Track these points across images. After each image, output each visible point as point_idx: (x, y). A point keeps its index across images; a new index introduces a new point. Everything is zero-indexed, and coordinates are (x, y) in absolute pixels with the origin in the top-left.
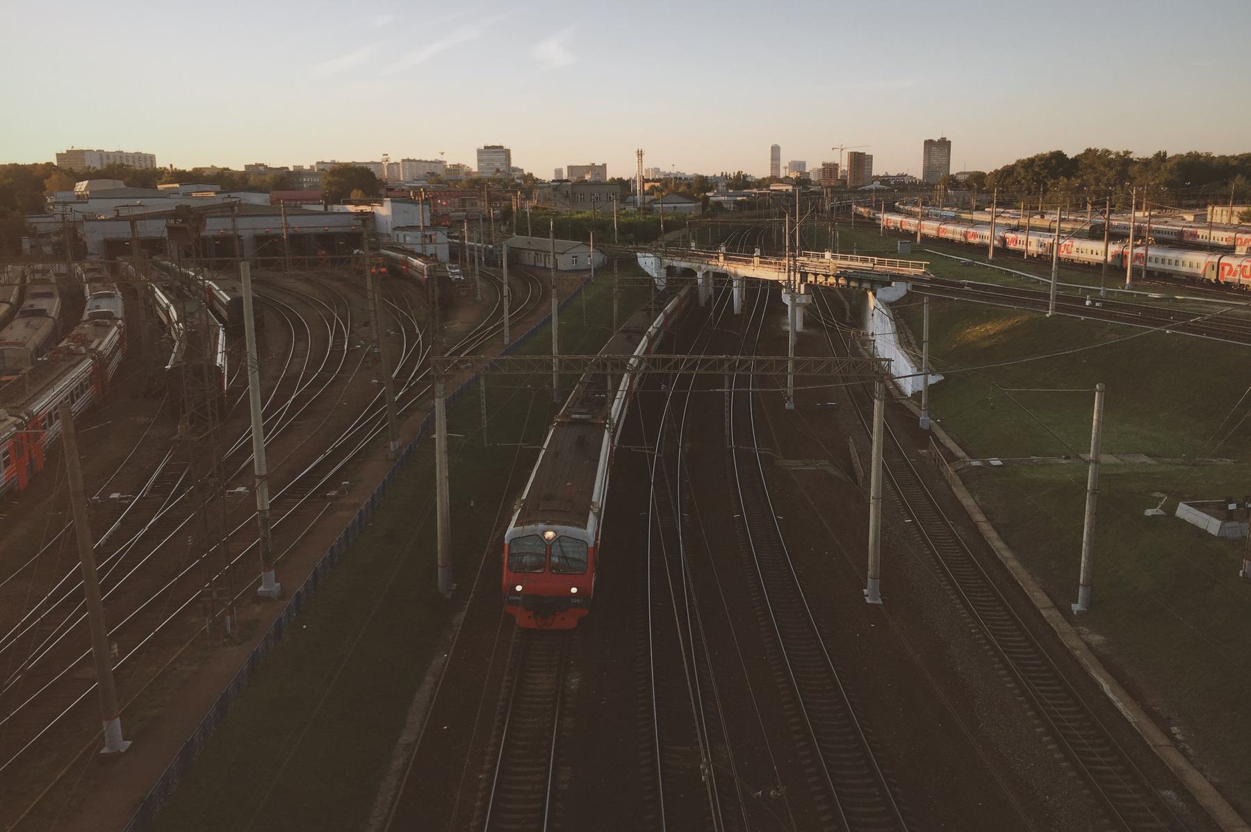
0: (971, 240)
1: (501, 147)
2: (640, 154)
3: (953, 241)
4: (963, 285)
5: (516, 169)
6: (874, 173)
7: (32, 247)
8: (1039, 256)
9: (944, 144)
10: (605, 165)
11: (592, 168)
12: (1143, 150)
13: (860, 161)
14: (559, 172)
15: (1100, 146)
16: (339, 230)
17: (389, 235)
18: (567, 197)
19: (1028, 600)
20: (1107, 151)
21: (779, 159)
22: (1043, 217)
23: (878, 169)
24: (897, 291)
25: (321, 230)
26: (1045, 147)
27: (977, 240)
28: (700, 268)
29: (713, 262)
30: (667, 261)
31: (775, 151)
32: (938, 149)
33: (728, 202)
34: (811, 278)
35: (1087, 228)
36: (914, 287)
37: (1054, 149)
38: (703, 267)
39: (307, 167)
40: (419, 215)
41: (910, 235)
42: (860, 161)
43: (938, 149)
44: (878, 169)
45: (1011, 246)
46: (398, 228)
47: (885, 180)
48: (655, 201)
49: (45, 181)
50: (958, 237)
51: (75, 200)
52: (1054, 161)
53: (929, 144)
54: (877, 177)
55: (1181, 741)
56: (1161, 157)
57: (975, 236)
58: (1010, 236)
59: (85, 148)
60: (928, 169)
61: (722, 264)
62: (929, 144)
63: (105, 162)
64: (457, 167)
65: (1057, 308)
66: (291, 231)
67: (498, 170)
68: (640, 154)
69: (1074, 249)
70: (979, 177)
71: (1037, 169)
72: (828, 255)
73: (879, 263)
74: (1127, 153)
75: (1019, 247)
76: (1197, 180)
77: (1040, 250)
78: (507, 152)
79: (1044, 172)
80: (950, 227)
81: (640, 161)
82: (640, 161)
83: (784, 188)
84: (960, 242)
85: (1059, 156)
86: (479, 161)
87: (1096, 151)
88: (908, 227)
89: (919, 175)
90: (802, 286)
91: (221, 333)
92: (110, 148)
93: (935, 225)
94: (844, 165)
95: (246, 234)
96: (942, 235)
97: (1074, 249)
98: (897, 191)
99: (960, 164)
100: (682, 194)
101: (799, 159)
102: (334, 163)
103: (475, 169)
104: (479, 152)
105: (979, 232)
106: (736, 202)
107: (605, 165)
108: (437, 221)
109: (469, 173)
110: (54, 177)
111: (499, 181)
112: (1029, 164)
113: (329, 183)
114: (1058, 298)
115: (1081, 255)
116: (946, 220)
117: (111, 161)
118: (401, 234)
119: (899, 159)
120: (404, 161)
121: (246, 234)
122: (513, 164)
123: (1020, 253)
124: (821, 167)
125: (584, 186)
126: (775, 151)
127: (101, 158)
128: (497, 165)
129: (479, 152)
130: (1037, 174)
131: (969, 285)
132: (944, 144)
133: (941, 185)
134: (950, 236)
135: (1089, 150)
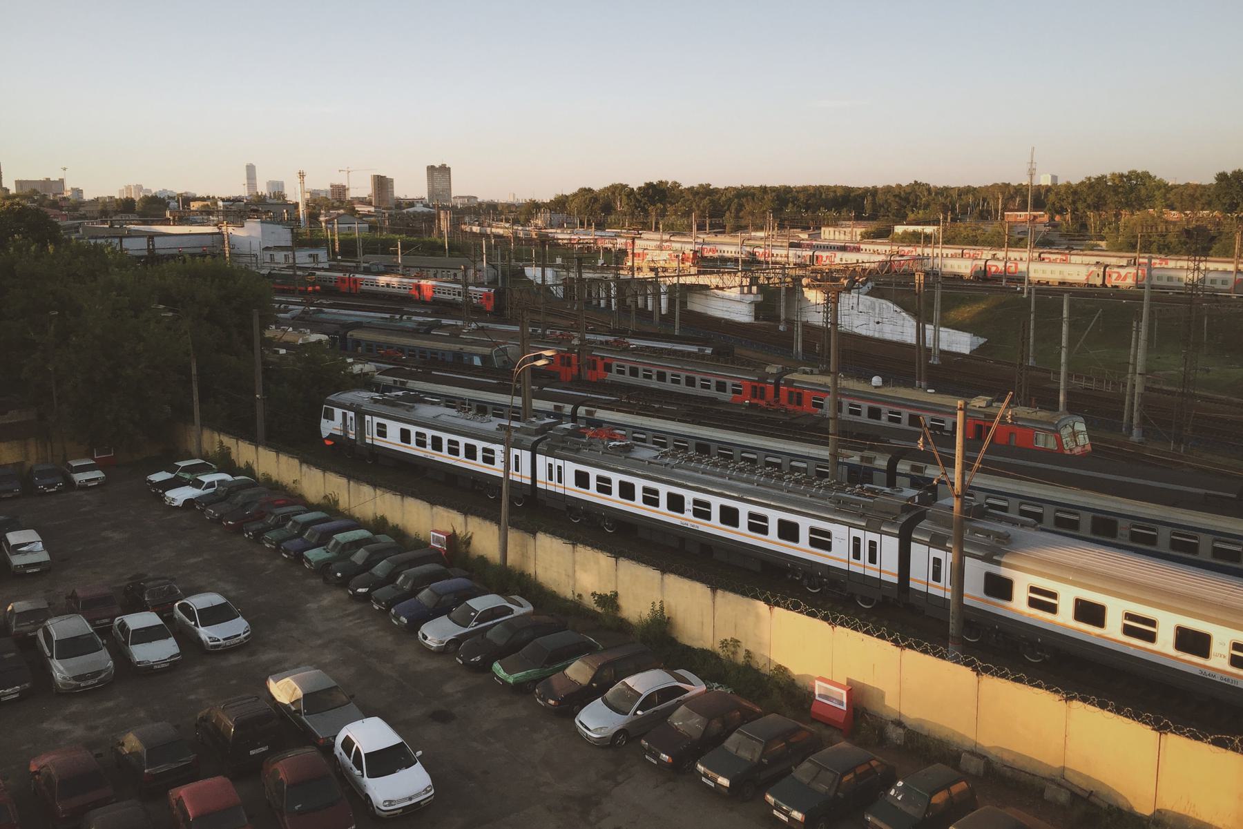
2: (302, 175)
21: (254, 178)
27: (716, 255)
31: (251, 170)
32: (439, 173)
46: (267, 249)
60: (432, 193)
62: (431, 169)
68: (302, 175)
81: (302, 182)
82: (302, 182)
126: (251, 170)
132: (445, 170)
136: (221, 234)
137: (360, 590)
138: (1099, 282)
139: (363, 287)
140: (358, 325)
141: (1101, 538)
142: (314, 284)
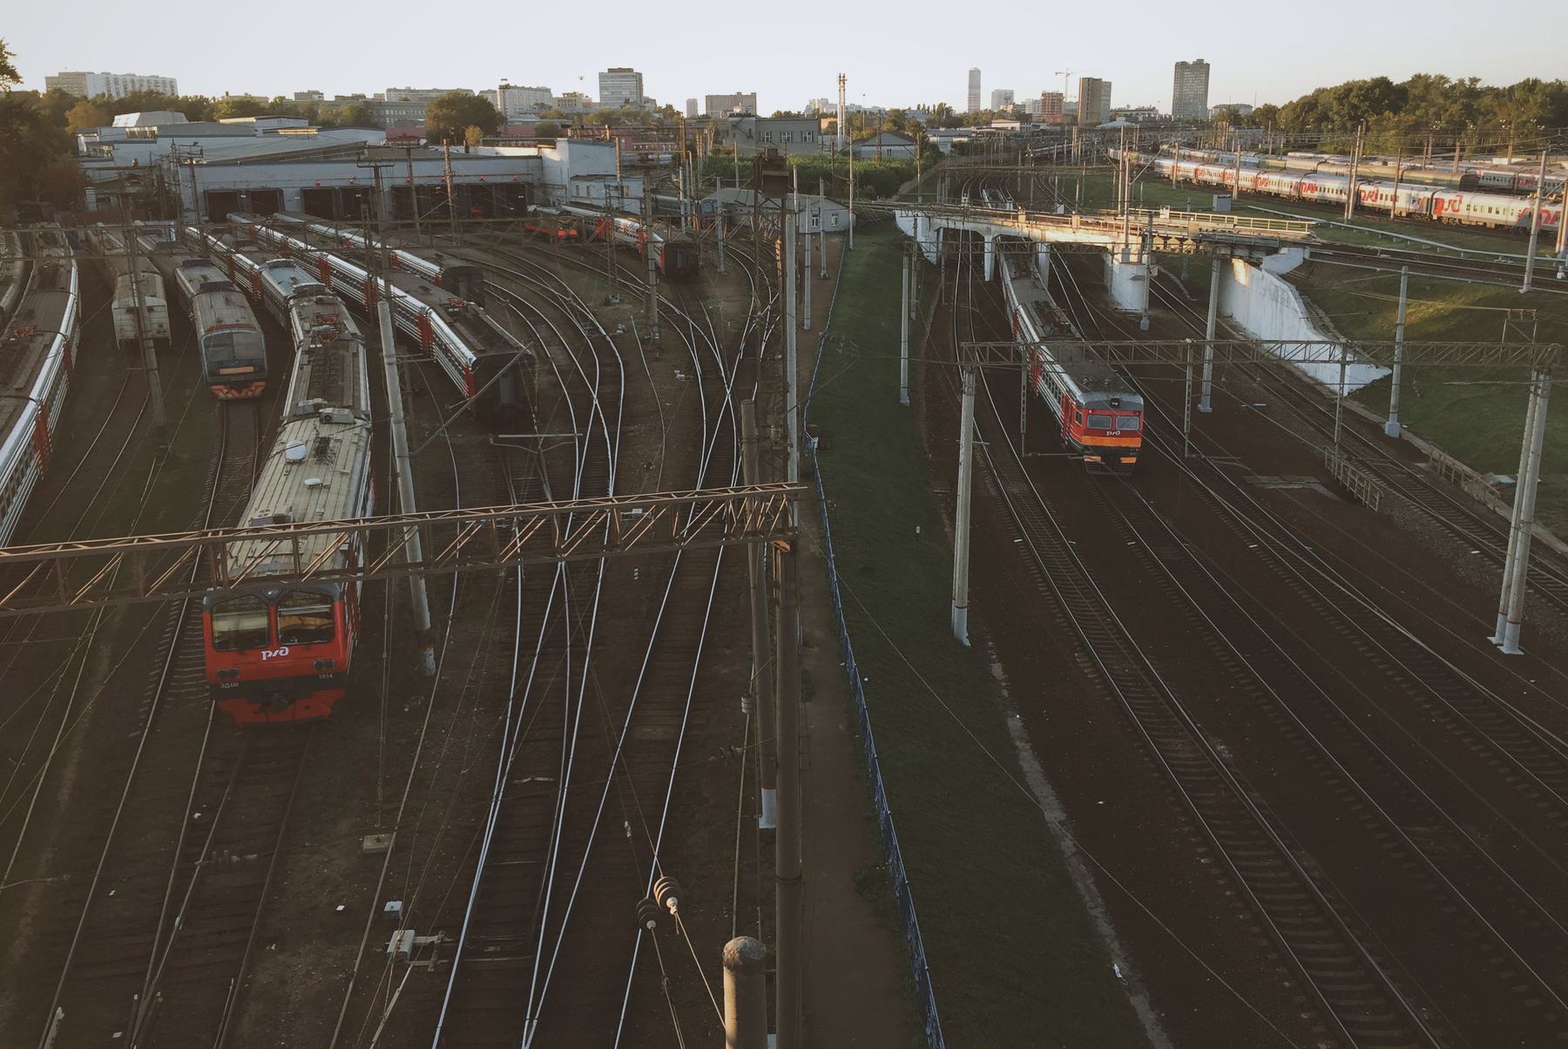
0: (1307, 194)
1: (630, 70)
2: (842, 80)
3: (1277, 195)
4: (1376, 252)
5: (648, 100)
6: (1114, 105)
7: (98, 200)
8: (1409, 215)
9: (1201, 68)
10: (754, 95)
11: (738, 98)
12: (1500, 74)
13: (1094, 89)
14: (692, 104)
15: (1433, 72)
16: (499, 180)
17: (564, 187)
19: (404, 402)
20: (1442, 77)
21: (979, 87)
22: (1385, 163)
23: (1117, 101)
24: (1291, 259)
25: (475, 180)
26: (1366, 73)
27: (1316, 195)
28: (989, 230)
29: (1008, 223)
30: (941, 222)
31: (975, 76)
32: (1192, 74)
33: (945, 143)
34: (1158, 242)
35: (1458, 179)
36: (1312, 254)
37: (1377, 75)
38: (993, 228)
40: (606, 160)
41: (1221, 188)
42: (1094, 89)
43: (1192, 74)
44: (1117, 101)
45: (1368, 202)
46: (577, 177)
47: (1130, 115)
48: (863, 141)
49: (67, 114)
50: (1285, 190)
51: (124, 137)
52: (1377, 91)
53: (1181, 67)
54: (1118, 112)
56: (1531, 86)
57: (1313, 188)
58: (1366, 188)
60: (1179, 102)
61: (1021, 226)
62: (1181, 67)
63: (130, 88)
64: (572, 98)
65: (1534, 282)
66: (457, 181)
67: (627, 101)
68: (842, 80)
69: (1463, 207)
70: (1269, 112)
71: (1355, 101)
72: (1165, 213)
73: (1240, 223)
74: (1474, 80)
75: (1380, 203)
77: (1412, 208)
78: (638, 78)
79: (1364, 106)
80: (1274, 178)
81: (842, 89)
82: (842, 89)
83: (1009, 125)
84: (1290, 196)
85: (1383, 83)
86: (602, 88)
87: (1427, 77)
88: (1207, 178)
89: (1165, 108)
91: (74, 270)
93: (1252, 174)
94: (1073, 95)
96: (1262, 188)
97: (1463, 207)
98: (1149, 131)
99: (1221, 93)
103: (596, 99)
104: (602, 76)
105: (1319, 183)
106: (954, 145)
107: (754, 95)
108: (639, 166)
109: (588, 105)
110: (78, 109)
111: (634, 116)
112: (1346, 93)
113: (436, 117)
114: (1535, 272)
115: (1472, 213)
116: (1204, 161)
117: (137, 86)
118: (583, 185)
119: (1144, 89)
122: (645, 94)
123: (1383, 213)
124: (1039, 97)
125: (734, 118)
126: (975, 76)
127: (108, 83)
128: (626, 94)
129: (602, 76)
130: (1355, 107)
131: (1383, 252)
132: (1201, 68)
133: (1192, 123)
134: (1273, 188)
135: (1418, 77)
136: (539, 158)
137: (249, 857)
138: (1294, 193)
139: (617, 235)
140: (800, 325)
141: (402, 466)
142: (567, 226)
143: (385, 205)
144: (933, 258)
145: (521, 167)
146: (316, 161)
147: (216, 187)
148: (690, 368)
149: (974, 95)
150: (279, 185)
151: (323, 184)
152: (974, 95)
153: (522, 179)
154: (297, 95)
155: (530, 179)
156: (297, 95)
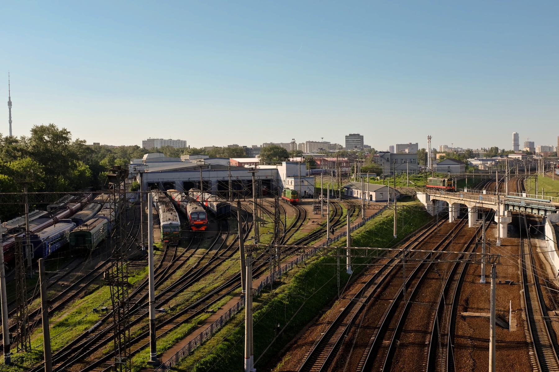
1: (358, 135)
2: (430, 138)
5: (367, 146)
11: (410, 146)
14: (392, 148)
18: (388, 161)
31: (516, 137)
39: (259, 146)
55: (124, 334)
59: (156, 138)
68: (430, 138)
76: (524, 168)
78: (362, 138)
90: (506, 213)
92: (166, 138)
95: (214, 180)
100: (454, 160)
101: (531, 140)
102: (272, 144)
120: (307, 142)
121: (214, 180)
126: (516, 137)
143: (214, 187)
144: (228, 244)
145: (269, 173)
146: (186, 171)
147: (152, 181)
148: (414, 231)
149: (516, 145)
150: (174, 180)
151: (191, 180)
152: (516, 145)
153: (269, 178)
154: (144, 142)
155: (272, 178)
156: (144, 142)
